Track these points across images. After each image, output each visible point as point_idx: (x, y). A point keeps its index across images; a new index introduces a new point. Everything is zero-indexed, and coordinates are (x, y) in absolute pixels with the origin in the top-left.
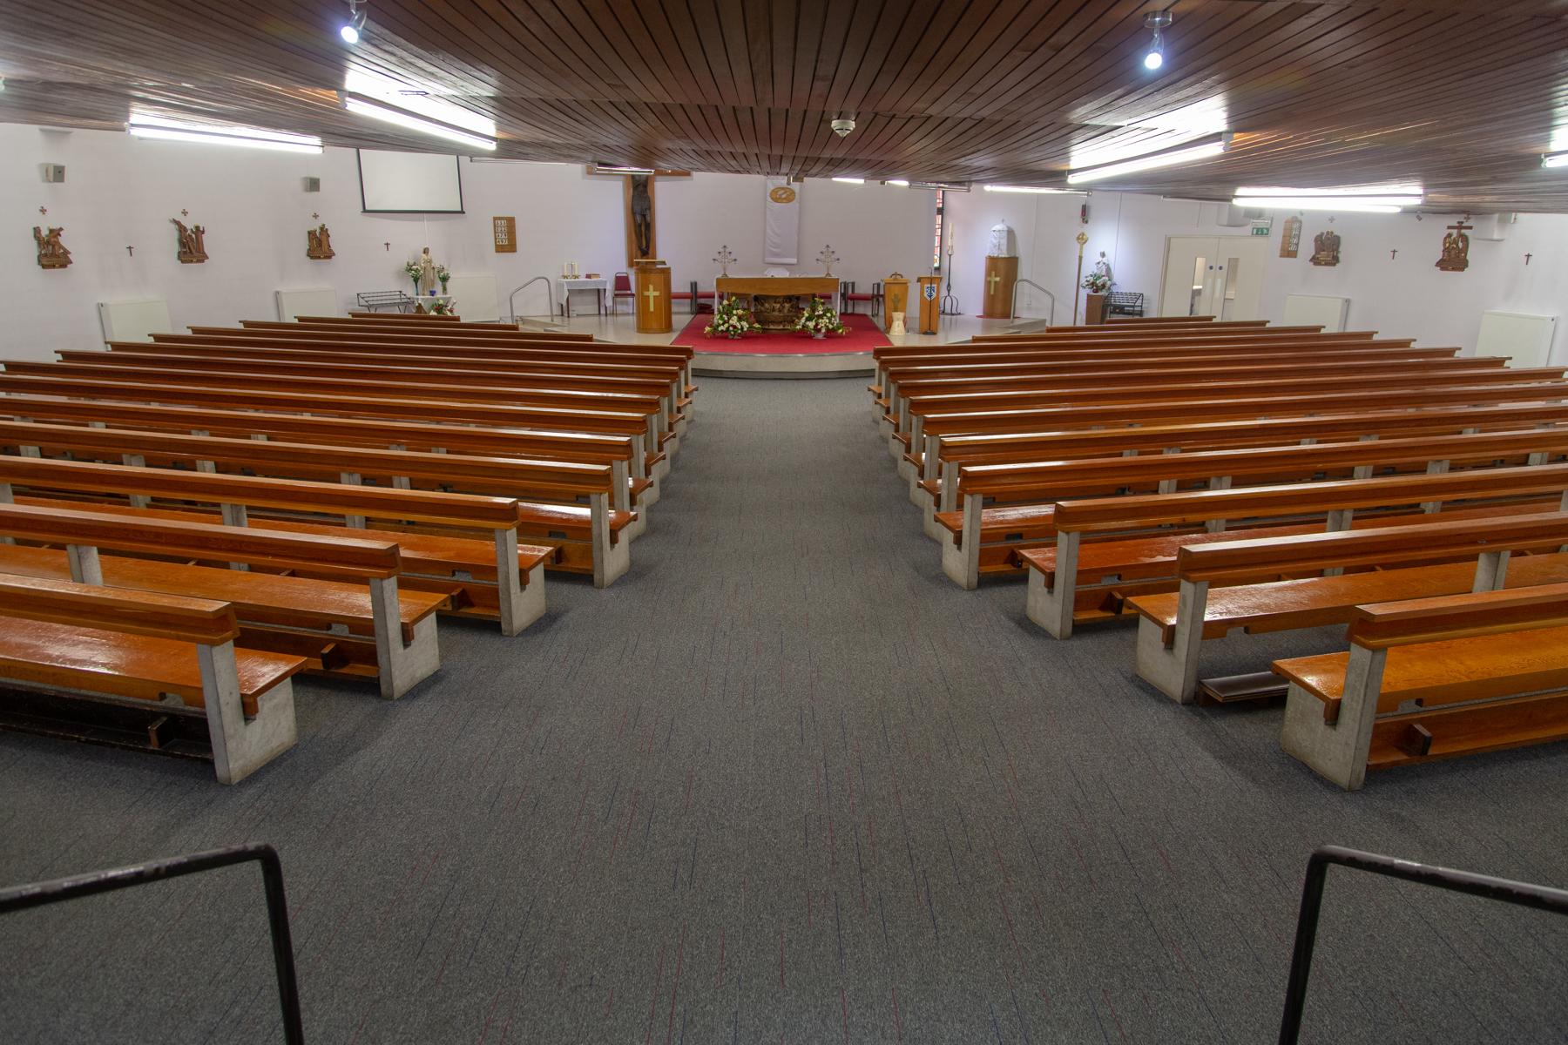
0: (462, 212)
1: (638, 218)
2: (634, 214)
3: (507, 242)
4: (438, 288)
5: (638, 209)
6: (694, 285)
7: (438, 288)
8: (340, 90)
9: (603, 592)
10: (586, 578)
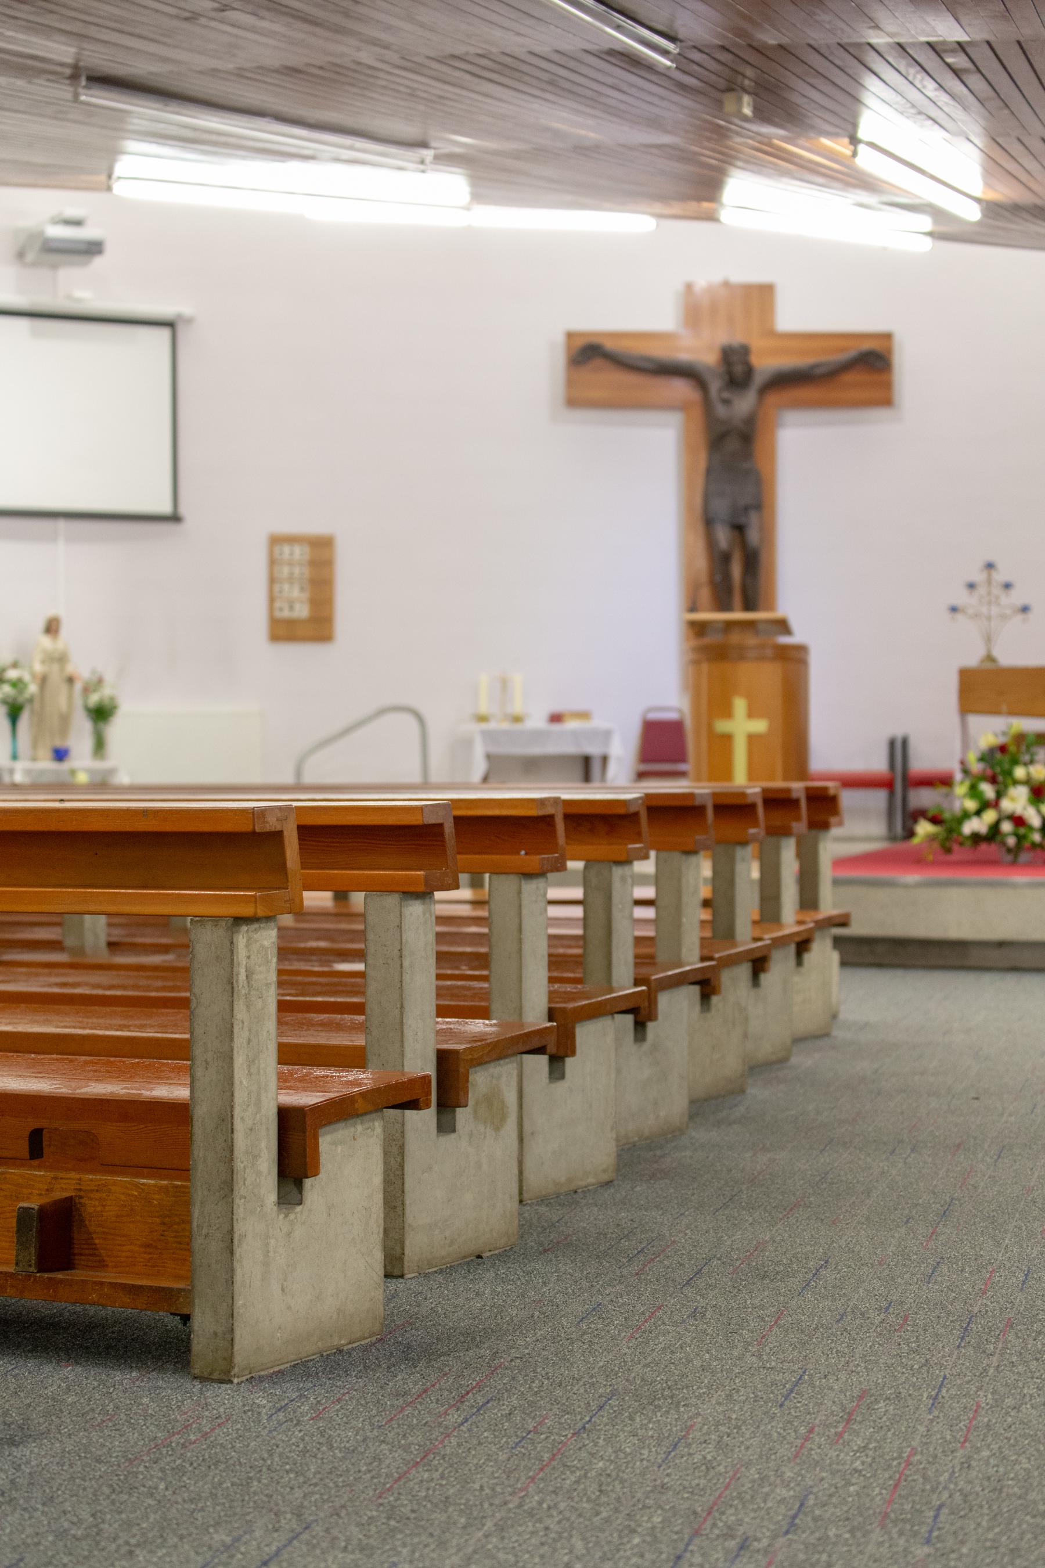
0: (175, 518)
1: (723, 536)
2: (709, 522)
3: (306, 621)
4: (80, 739)
5: (721, 507)
6: (899, 749)
7: (80, 739)
8: (854, 141)
9: (222, 1398)
10: (158, 1338)
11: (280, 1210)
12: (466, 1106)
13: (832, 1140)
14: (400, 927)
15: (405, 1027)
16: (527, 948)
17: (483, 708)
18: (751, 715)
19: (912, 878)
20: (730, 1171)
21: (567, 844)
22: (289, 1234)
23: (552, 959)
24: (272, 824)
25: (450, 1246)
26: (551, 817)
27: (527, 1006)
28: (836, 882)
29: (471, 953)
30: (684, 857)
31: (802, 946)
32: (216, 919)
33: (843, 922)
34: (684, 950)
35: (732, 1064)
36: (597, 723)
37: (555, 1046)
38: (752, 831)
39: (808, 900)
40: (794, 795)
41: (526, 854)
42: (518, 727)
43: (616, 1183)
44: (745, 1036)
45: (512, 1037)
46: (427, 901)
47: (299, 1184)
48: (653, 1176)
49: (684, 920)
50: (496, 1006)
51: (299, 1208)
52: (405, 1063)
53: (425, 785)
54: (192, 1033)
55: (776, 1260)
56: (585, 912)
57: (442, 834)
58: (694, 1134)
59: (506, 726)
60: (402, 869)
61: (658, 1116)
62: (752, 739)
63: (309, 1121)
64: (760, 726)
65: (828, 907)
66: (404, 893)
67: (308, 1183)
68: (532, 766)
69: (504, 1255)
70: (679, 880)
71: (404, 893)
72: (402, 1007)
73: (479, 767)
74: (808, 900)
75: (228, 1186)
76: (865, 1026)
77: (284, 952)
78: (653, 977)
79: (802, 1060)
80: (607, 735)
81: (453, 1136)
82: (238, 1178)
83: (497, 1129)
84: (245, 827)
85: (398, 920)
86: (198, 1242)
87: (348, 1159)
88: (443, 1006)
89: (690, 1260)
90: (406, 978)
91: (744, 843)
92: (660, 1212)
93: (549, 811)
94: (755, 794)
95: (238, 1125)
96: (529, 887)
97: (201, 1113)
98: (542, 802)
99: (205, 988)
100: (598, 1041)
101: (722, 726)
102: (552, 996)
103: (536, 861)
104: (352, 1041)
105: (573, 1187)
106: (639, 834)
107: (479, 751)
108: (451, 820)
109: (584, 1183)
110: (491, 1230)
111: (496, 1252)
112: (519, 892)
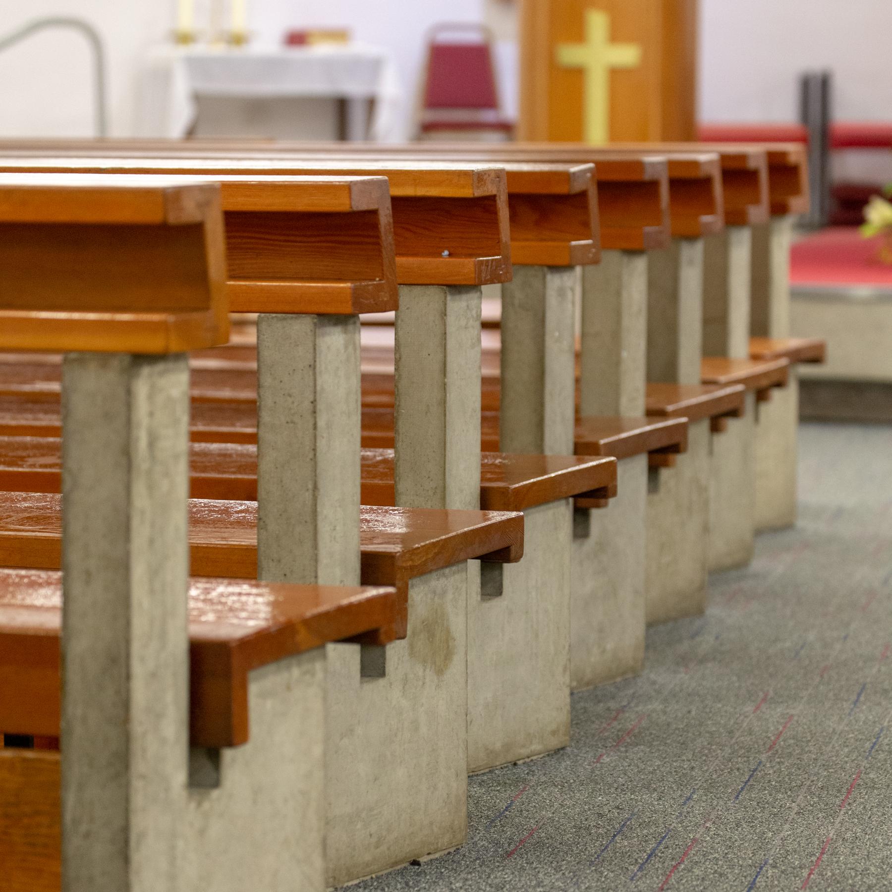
6: (816, 91)
11: (190, 795)
12: (403, 638)
13: (863, 688)
14: (313, 367)
15: (320, 518)
16: (452, 397)
17: (187, 22)
18: (616, 36)
19: (862, 289)
20: (731, 732)
21: (512, 239)
22: (202, 832)
23: (367, 410)
24: (189, 212)
25: (377, 847)
26: (492, 198)
27: (453, 485)
28: (796, 295)
29: (230, 401)
30: (625, 259)
31: (762, 395)
32: (104, 357)
33: (814, 356)
34: (624, 401)
35: (686, 572)
36: (360, 46)
37: (497, 557)
38: (706, 219)
39: (760, 327)
40: (752, 164)
41: (450, 255)
42: (237, 52)
43: (569, 749)
44: (706, 529)
45: (465, 533)
46: (350, 327)
47: (214, 756)
48: (619, 740)
49: (625, 354)
50: (405, 486)
51: (215, 793)
52: (320, 573)
53: (100, 145)
54: (65, 529)
55: (860, 868)
56: (503, 342)
57: (375, 226)
58: (652, 676)
59: (219, 50)
60: (312, 279)
61: (604, 651)
62: (616, 74)
63: (236, 662)
64: (627, 55)
65: (785, 337)
66: (320, 315)
67: (228, 754)
68: (261, 114)
69: (451, 859)
70: (618, 294)
71: (320, 315)
72: (315, 488)
73: (180, 115)
74: (760, 327)
75: (121, 761)
76: (839, 513)
77: (200, 407)
78: (602, 442)
79: (773, 565)
80: (374, 66)
81: (382, 682)
82: (136, 747)
83: (440, 672)
84: (150, 215)
85: (310, 356)
86: (74, 844)
87: (282, 709)
88: (205, 480)
89: (732, 867)
90: (322, 444)
91: (691, 238)
92: (655, 795)
93: (489, 189)
94: (710, 163)
95: (138, 670)
96: (457, 305)
97: (80, 651)
98: (479, 177)
99: (87, 462)
100: (546, 529)
101: (570, 55)
102: (486, 471)
103: (466, 266)
104: (223, 538)
105: (511, 758)
106: (586, 224)
107: (181, 90)
108: (388, 204)
109: (524, 752)
110: (431, 824)
111: (437, 855)
112: (444, 314)
